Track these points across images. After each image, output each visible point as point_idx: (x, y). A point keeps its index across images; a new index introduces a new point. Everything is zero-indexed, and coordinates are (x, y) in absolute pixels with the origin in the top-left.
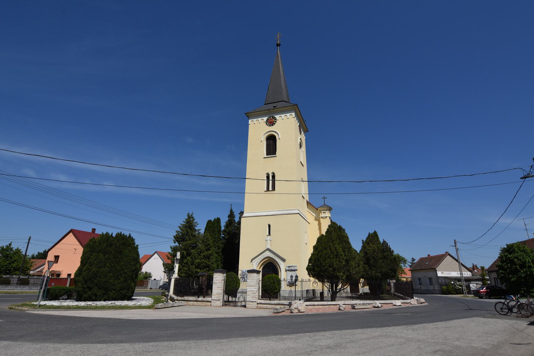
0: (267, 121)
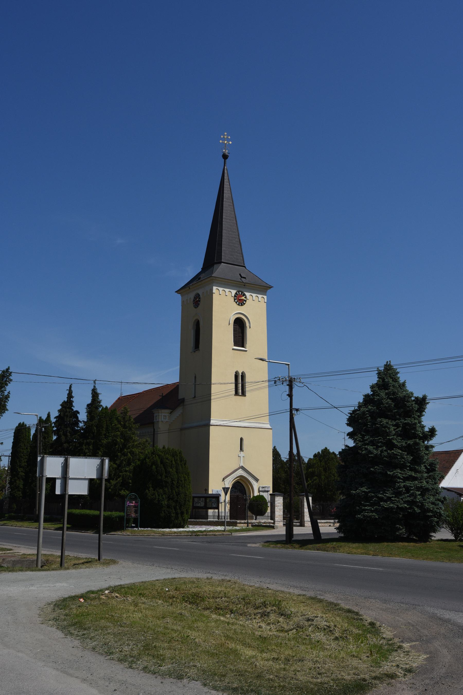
0: (235, 296)
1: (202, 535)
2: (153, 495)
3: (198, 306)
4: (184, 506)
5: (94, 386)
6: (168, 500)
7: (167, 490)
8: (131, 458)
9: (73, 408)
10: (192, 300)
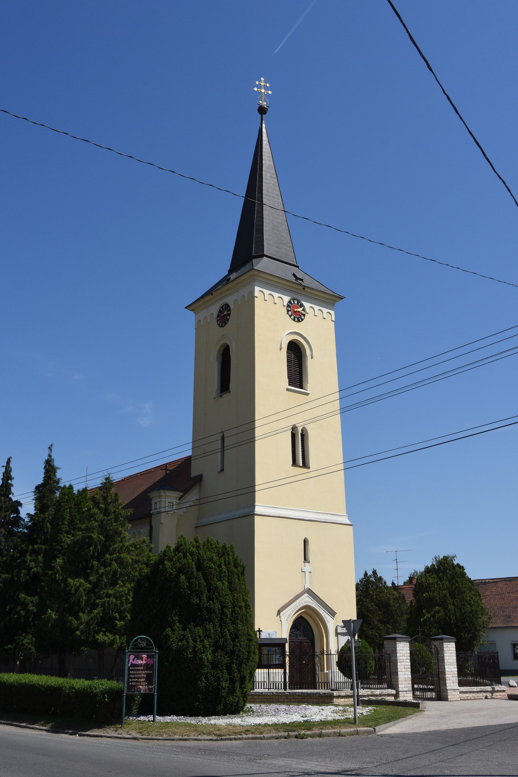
0: (288, 306)
1: (312, 736)
2: (181, 640)
3: (225, 324)
4: (246, 665)
5: (50, 456)
6: (214, 650)
7: (211, 628)
8: (117, 570)
9: (10, 496)
10: (215, 316)
